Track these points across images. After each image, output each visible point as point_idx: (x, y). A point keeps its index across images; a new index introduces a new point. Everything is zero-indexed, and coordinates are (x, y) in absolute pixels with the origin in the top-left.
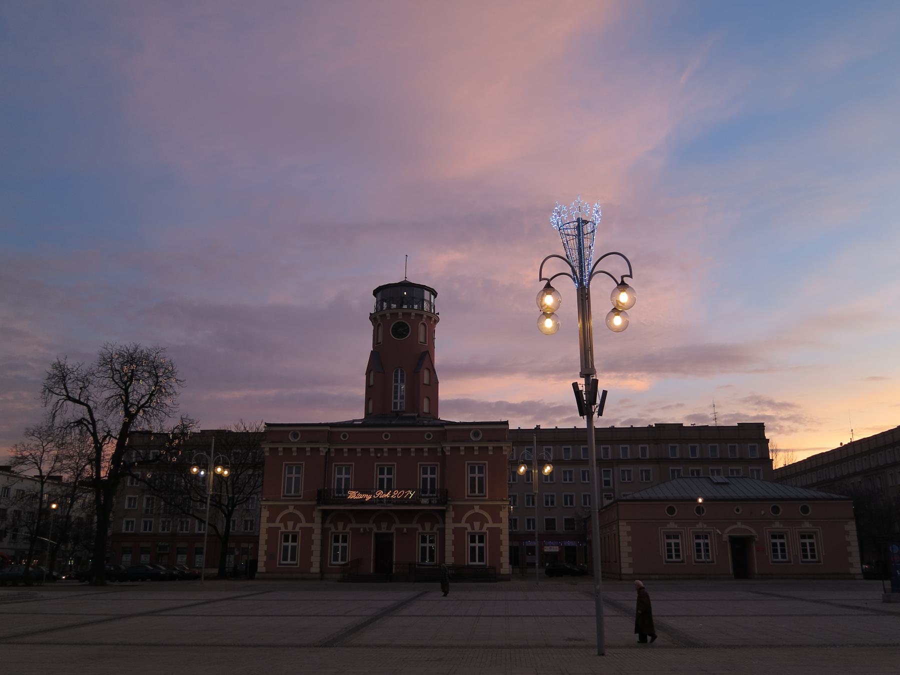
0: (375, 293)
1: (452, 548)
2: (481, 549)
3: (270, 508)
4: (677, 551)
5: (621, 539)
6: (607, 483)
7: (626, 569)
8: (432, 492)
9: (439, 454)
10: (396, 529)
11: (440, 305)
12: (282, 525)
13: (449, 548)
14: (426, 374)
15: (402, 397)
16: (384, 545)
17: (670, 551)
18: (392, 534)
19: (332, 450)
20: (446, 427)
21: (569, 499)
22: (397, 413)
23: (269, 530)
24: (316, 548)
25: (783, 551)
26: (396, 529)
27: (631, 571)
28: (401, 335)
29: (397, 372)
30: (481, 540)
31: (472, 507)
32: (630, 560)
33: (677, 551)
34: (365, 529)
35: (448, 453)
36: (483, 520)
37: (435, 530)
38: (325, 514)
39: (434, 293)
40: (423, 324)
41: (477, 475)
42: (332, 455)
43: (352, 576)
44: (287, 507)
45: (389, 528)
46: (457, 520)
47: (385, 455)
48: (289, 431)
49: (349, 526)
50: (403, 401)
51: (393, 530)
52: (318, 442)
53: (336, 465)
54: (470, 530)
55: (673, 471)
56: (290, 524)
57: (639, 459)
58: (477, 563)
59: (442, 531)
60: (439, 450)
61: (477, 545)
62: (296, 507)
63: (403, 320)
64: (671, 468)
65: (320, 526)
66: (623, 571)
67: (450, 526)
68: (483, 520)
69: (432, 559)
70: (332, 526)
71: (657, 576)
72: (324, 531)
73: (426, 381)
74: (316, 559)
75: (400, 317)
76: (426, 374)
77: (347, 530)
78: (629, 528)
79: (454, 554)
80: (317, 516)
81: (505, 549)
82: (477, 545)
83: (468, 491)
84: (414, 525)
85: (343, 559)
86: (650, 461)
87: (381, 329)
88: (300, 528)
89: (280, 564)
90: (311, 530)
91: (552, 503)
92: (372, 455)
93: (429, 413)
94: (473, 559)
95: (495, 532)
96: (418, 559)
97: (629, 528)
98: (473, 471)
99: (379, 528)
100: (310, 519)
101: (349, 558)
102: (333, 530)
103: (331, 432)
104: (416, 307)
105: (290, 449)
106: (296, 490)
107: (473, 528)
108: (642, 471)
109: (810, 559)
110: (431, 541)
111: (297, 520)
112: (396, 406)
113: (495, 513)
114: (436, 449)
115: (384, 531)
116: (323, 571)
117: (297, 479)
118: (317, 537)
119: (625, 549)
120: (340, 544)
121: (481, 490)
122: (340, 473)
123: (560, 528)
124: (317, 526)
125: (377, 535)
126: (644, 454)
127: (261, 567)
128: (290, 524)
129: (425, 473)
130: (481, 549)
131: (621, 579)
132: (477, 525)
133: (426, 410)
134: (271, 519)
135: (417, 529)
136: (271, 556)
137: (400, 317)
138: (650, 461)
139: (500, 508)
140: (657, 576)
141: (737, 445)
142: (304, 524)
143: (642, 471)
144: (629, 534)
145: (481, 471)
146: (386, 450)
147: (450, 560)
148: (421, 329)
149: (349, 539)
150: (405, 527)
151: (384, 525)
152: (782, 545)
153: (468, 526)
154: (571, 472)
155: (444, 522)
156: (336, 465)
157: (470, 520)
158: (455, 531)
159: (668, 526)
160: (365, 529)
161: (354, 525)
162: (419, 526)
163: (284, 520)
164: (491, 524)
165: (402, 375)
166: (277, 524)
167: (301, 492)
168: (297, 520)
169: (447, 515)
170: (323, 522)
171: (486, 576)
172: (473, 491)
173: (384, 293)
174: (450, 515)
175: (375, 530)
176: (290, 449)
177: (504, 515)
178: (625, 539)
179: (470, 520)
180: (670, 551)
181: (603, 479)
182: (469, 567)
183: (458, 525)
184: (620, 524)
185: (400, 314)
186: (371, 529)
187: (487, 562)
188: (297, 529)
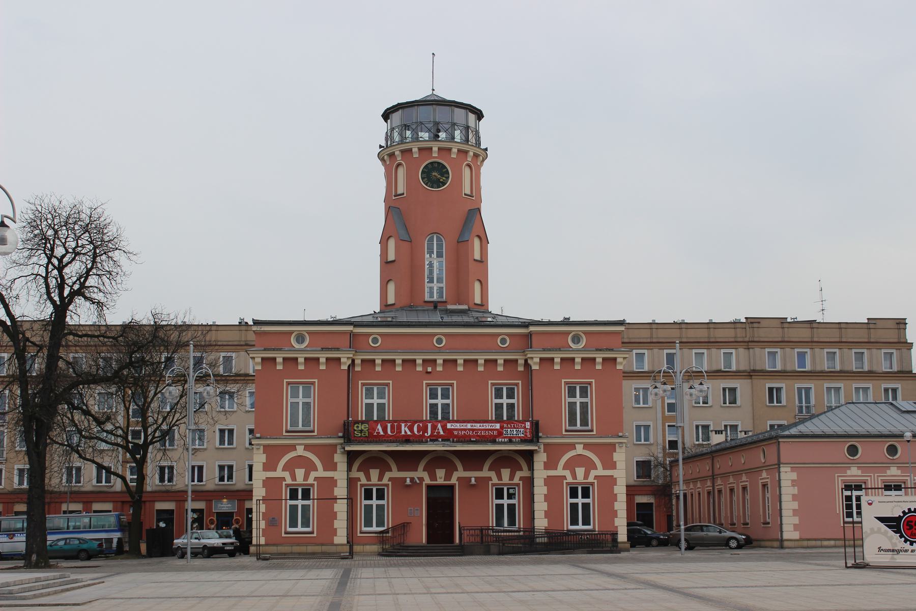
0: (386, 115)
1: (545, 506)
2: (586, 507)
5: (783, 490)
6: (672, 407)
7: (790, 533)
9: (521, 368)
10: (459, 479)
11: (488, 132)
12: (287, 475)
13: (540, 506)
15: (440, 280)
16: (440, 504)
18: (452, 487)
19: (358, 362)
20: (532, 329)
22: (435, 305)
23: (267, 482)
24: (341, 508)
26: (459, 479)
27: (796, 535)
28: (439, 183)
29: (431, 240)
30: (586, 494)
31: (572, 446)
32: (796, 520)
34: (412, 479)
35: (535, 367)
37: (516, 480)
38: (352, 457)
39: (479, 115)
40: (469, 165)
42: (358, 369)
43: (395, 547)
44: (293, 448)
45: (448, 477)
46: (550, 464)
47: (439, 369)
48: (291, 333)
49: (388, 475)
50: (443, 285)
51: (454, 481)
53: (363, 385)
54: (289, 481)
56: (300, 473)
57: (720, 371)
58: (580, 527)
59: (529, 482)
60: (521, 362)
61: (580, 501)
62: (307, 447)
63: (432, 156)
65: (344, 475)
66: (786, 536)
67: (540, 474)
68: (590, 466)
69: (512, 522)
70: (361, 475)
71: (832, 543)
72: (352, 483)
73: (477, 256)
74: (341, 524)
75: (435, 155)
77: (385, 481)
78: (794, 476)
80: (340, 459)
82: (580, 501)
83: (565, 424)
84: (485, 473)
85: (380, 523)
86: (737, 374)
87: (401, 172)
88: (316, 479)
89: (286, 533)
90: (333, 482)
92: (419, 369)
94: (574, 521)
96: (492, 522)
97: (794, 476)
98: (572, 393)
99: (433, 477)
100: (330, 465)
101: (389, 522)
102: (364, 481)
103: (351, 331)
104: (442, 135)
105: (295, 360)
106: (306, 422)
107: (574, 477)
110: (510, 496)
111: (310, 467)
112: (431, 293)
113: (606, 453)
114: (516, 361)
115: (440, 481)
116: (351, 542)
117: (307, 405)
118: (341, 491)
119: (789, 505)
120: (374, 502)
121: (584, 422)
122: (369, 394)
124: (340, 475)
125: (429, 487)
126: (728, 363)
127: (258, 537)
128: (580, 472)
129: (499, 395)
130: (586, 507)
131: (782, 547)
133: (478, 300)
134: (268, 467)
135: (490, 479)
136: (273, 522)
137: (435, 155)
138: (737, 374)
139: (612, 447)
140: (826, 543)
141: (837, 351)
142: (321, 473)
144: (794, 483)
145: (584, 393)
146: (440, 362)
147: (541, 523)
148: (467, 172)
149: (389, 493)
150: (473, 475)
151: (441, 473)
153: (567, 473)
155: (531, 468)
156: (363, 385)
157: (571, 465)
158: (548, 481)
160: (412, 479)
161: (396, 473)
162: (492, 474)
163: (290, 467)
165: (440, 246)
166: (279, 473)
167: (314, 425)
168: (310, 467)
169: (535, 459)
170: (349, 469)
171: (600, 544)
172: (572, 421)
174: (540, 459)
175: (427, 481)
176: (295, 360)
177: (619, 456)
178: (788, 491)
179: (571, 465)
184: (782, 469)
185: (435, 149)
186: (421, 479)
187: (595, 525)
188: (311, 481)
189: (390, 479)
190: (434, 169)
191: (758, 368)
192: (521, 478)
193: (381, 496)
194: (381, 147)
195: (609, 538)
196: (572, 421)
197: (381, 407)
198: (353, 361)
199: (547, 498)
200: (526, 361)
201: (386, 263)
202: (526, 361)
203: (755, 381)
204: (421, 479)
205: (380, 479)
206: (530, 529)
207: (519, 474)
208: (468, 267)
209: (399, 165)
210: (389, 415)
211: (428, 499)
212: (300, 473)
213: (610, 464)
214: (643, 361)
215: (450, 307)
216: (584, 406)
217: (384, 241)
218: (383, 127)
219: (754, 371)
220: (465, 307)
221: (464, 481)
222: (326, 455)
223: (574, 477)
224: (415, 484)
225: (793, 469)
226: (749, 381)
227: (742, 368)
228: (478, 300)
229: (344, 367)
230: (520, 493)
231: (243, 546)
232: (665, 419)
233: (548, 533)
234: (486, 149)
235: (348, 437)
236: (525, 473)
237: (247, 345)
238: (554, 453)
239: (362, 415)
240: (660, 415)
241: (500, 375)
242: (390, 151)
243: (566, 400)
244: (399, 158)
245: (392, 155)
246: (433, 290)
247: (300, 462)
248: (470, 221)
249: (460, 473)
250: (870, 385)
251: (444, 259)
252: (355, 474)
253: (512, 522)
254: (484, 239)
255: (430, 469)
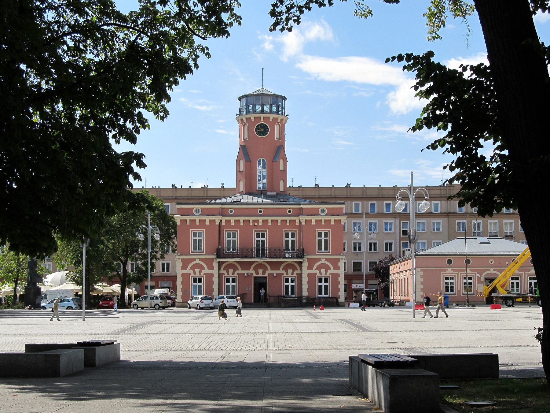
1: (307, 286)
2: (326, 287)
3: (183, 260)
4: (452, 287)
8: (293, 249)
10: (268, 274)
13: (305, 286)
14: (282, 162)
17: (447, 287)
18: (266, 277)
21: (372, 246)
23: (309, 275)
25: (517, 287)
26: (268, 274)
30: (326, 281)
33: (452, 287)
34: (247, 274)
35: (304, 223)
36: (328, 268)
37: (295, 274)
38: (220, 264)
41: (323, 239)
51: (266, 275)
52: (214, 216)
55: (459, 223)
57: (431, 213)
58: (323, 295)
59: (300, 275)
60: (297, 221)
61: (323, 284)
64: (457, 221)
69: (293, 293)
70: (225, 272)
72: (221, 275)
76: (282, 162)
78: (422, 273)
79: (308, 290)
80: (215, 265)
81: (341, 287)
82: (323, 284)
86: (442, 215)
87: (246, 128)
91: (359, 249)
93: (284, 192)
94: (320, 293)
95: (336, 276)
96: (284, 292)
97: (422, 273)
99: (257, 273)
102: (226, 274)
107: (321, 273)
108: (434, 223)
109: (450, 292)
110: (292, 282)
115: (260, 275)
118: (216, 279)
120: (231, 284)
121: (326, 248)
123: (365, 269)
124: (215, 272)
125: (255, 277)
130: (326, 287)
132: (323, 271)
134: (309, 268)
137: (262, 120)
138: (442, 215)
139: (338, 260)
142: (207, 271)
143: (434, 223)
147: (305, 294)
150: (275, 272)
152: (517, 283)
154: (375, 224)
155: (301, 269)
159: (447, 272)
164: (332, 271)
168: (328, 268)
170: (219, 269)
171: (332, 303)
172: (320, 248)
173: (251, 100)
174: (305, 265)
177: (341, 264)
180: (447, 287)
181: (402, 229)
182: (320, 298)
183: (185, 271)
186: (252, 274)
187: (329, 295)
189: (238, 274)
190: (259, 129)
191: (452, 211)
192: (297, 274)
193: (234, 281)
194: (237, 115)
195: (335, 301)
196: (320, 248)
197: (234, 241)
198: (221, 221)
199: (213, 283)
200: (300, 221)
201: (238, 172)
202: (300, 221)
203: (450, 219)
204: (252, 274)
205: (233, 273)
206: (300, 297)
207: (296, 272)
208: (278, 173)
209: (245, 124)
210: (237, 245)
211: (255, 283)
212: (197, 271)
213: (337, 267)
214: (389, 207)
215: (268, 193)
216: (326, 241)
217: (238, 162)
218: (238, 104)
219: (450, 213)
220: (275, 193)
221: (271, 275)
222: (209, 263)
223: (321, 273)
224: (250, 275)
225: (422, 270)
226: (447, 219)
227: (443, 211)
228: (282, 189)
229: (217, 223)
230: (296, 280)
231: (173, 305)
232: (401, 239)
233: (308, 298)
234: (288, 115)
235: (218, 256)
236: (298, 271)
237: (176, 199)
238: (311, 263)
239: (225, 245)
240: (398, 237)
241: (288, 227)
242: (241, 118)
243: (317, 239)
244: (245, 121)
245: (242, 120)
246: (262, 183)
247: (198, 266)
248: (279, 150)
249: (269, 271)
250: (513, 221)
251: (266, 170)
252: (222, 271)
253: (293, 293)
254: (285, 161)
255: (256, 269)
